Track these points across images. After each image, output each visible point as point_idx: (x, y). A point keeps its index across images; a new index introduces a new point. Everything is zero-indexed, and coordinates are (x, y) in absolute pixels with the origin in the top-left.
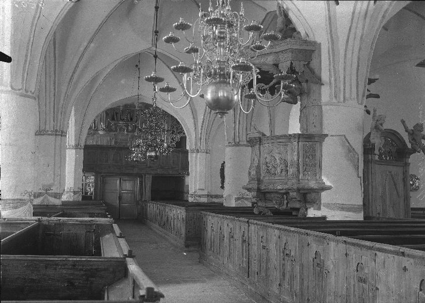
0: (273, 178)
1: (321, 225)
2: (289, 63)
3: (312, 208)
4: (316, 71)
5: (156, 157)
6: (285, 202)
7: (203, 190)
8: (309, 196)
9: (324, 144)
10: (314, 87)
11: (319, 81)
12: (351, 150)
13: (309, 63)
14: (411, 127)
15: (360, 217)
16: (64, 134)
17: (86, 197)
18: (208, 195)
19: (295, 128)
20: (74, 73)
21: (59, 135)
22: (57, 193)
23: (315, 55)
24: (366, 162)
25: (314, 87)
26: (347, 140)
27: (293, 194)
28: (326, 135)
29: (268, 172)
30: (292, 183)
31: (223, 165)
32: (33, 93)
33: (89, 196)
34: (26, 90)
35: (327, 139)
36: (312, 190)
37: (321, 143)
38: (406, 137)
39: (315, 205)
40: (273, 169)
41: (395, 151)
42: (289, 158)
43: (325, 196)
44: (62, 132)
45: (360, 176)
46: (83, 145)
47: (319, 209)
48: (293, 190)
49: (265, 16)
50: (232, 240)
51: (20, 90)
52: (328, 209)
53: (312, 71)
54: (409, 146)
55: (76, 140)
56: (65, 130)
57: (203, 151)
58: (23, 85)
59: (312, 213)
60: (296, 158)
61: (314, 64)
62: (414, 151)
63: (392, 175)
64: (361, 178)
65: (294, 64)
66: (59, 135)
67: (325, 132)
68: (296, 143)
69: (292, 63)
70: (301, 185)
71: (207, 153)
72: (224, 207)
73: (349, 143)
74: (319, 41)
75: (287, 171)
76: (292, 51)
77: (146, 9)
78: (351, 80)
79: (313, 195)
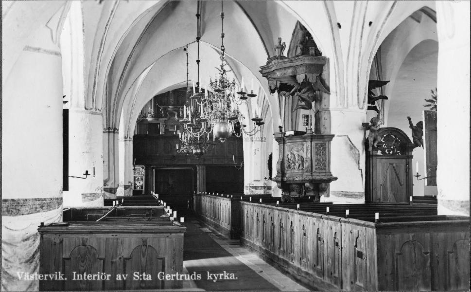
0: (293, 171)
1: (338, 210)
2: (304, 75)
3: (323, 196)
4: (326, 82)
5: (201, 153)
6: (304, 191)
7: (259, 181)
8: (321, 185)
9: (332, 142)
10: (325, 95)
11: (328, 90)
12: (352, 147)
13: (321, 75)
14: (415, 124)
15: (362, 201)
16: (116, 131)
17: (136, 192)
18: (264, 187)
19: (287, 134)
20: (124, 70)
21: (112, 132)
22: (112, 188)
23: (325, 68)
24: (368, 157)
25: (325, 95)
26: (349, 139)
27: (307, 184)
28: (333, 136)
29: (289, 167)
30: (307, 176)
31: (271, 156)
32: (100, 111)
33: (138, 191)
34: (95, 108)
35: (334, 139)
36: (322, 181)
37: (329, 141)
38: (409, 134)
39: (325, 193)
40: (293, 164)
41: (399, 145)
42: (304, 156)
43: (333, 186)
44: (115, 129)
45: (360, 168)
46: (132, 137)
47: (328, 196)
48: (307, 181)
49: (295, 26)
50: (282, 229)
51: (91, 109)
52: (333, 196)
53: (323, 81)
54: (412, 139)
55: (125, 132)
56: (117, 127)
57: (258, 139)
58: (93, 106)
59: (323, 199)
60: (309, 156)
61: (324, 75)
62: (416, 145)
63: (394, 167)
64: (361, 170)
65: (308, 77)
66: (112, 132)
67: (332, 133)
68: (310, 142)
69: (306, 76)
70: (313, 177)
71: (262, 141)
72: (272, 197)
73: (351, 142)
74: (327, 57)
75: (303, 166)
76: (306, 66)
78: (352, 90)
79: (323, 185)
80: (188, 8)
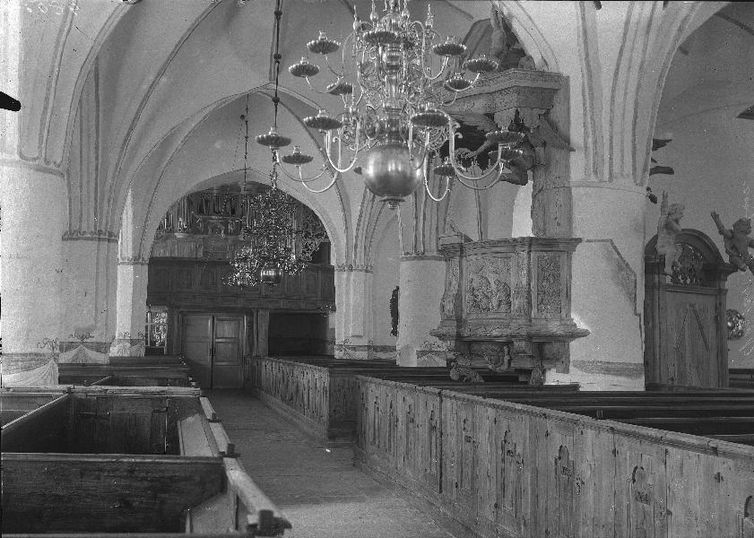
0: (484, 316)
1: (570, 399)
2: (512, 111)
3: (554, 370)
4: (560, 125)
5: (277, 278)
6: (506, 358)
7: (361, 337)
8: (548, 348)
9: (575, 255)
10: (557, 155)
11: (566, 145)
12: (622, 266)
13: (548, 112)
14: (728, 226)
15: (638, 385)
16: (113, 238)
17: (152, 350)
18: (369, 347)
20: (131, 129)
21: (104, 239)
22: (102, 343)
23: (559, 98)
24: (650, 288)
25: (557, 155)
26: (615, 248)
27: (520, 345)
28: (579, 240)
29: (476, 305)
30: (518, 326)
31: (396, 293)
32: (59, 166)
33: (158, 349)
34: (45, 160)
35: (579, 247)
36: (553, 338)
37: (569, 254)
38: (720, 243)
39: (559, 364)
40: (485, 300)
41: (701, 268)
42: (513, 281)
43: (576, 349)
44: (111, 234)
45: (638, 312)
46: (147, 257)
47: (566, 371)
48: (521, 338)
49: (470, 28)
50: (411, 426)
51: (35, 159)
52: (582, 372)
53: (554, 126)
54: (726, 259)
55: (134, 248)
56: (115, 231)
57: (360, 268)
58: (41, 152)
59: (553, 378)
60: (524, 281)
61: (557, 114)
62: (734, 268)
63: (695, 311)
64: (640, 315)
65: (521, 114)
66: (104, 239)
67: (577, 234)
68: (525, 254)
69: (517, 112)
70: (535, 328)
71: (367, 271)
72: (398, 367)
73: (619, 254)
74: (565, 74)
75: (509, 304)
76: (519, 90)
78: (622, 142)
79: (556, 346)
80: (259, 16)
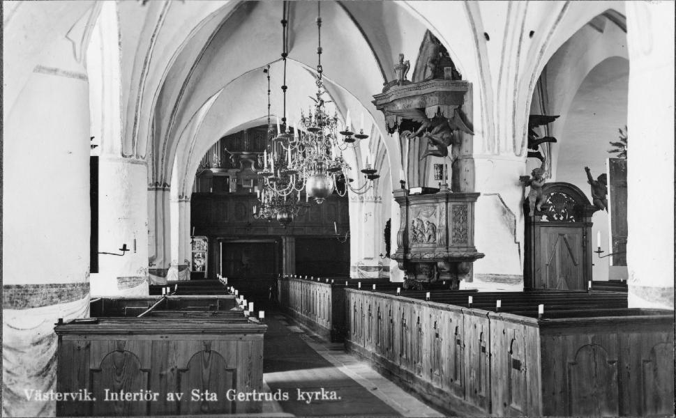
0: (420, 245)
1: (484, 301)
2: (436, 107)
3: (464, 280)
4: (469, 117)
5: (289, 220)
6: (436, 273)
7: (372, 259)
8: (461, 265)
9: (476, 204)
10: (466, 136)
11: (470, 128)
12: (506, 210)
13: (460, 107)
14: (595, 178)
15: (519, 288)
16: (167, 187)
17: (195, 275)
18: (380, 268)
20: (178, 100)
21: (160, 189)
22: (161, 269)
23: (467, 97)
24: (529, 225)
25: (466, 136)
26: (501, 199)
27: (440, 264)
28: (478, 194)
29: (415, 239)
30: (441, 252)
31: (389, 223)
32: (144, 159)
33: (199, 273)
34: (137, 155)
35: (479, 198)
36: (462, 259)
37: (473, 202)
38: (587, 191)
39: (466, 277)
40: (420, 235)
41: (572, 208)
42: (437, 223)
43: (478, 266)
44: (165, 185)
45: (517, 241)
46: (189, 195)
47: (471, 280)
48: (441, 259)
49: (423, 38)
50: (404, 328)
51: (131, 156)
52: (478, 281)
53: (463, 117)
54: (591, 199)
55: (179, 188)
56: (168, 182)
57: (370, 200)
58: (133, 151)
59: (464, 285)
60: (444, 223)
61: (466, 108)
62: (597, 208)
63: (565, 239)
64: (519, 243)
65: (442, 110)
66: (160, 189)
67: (477, 191)
68: (444, 204)
69: (439, 109)
70: (450, 253)
71: (376, 202)
72: (391, 282)
73: (503, 203)
74: (470, 82)
75: (435, 237)
76: (439, 94)
77: (270, 11)
78: (506, 129)
79: (464, 265)
